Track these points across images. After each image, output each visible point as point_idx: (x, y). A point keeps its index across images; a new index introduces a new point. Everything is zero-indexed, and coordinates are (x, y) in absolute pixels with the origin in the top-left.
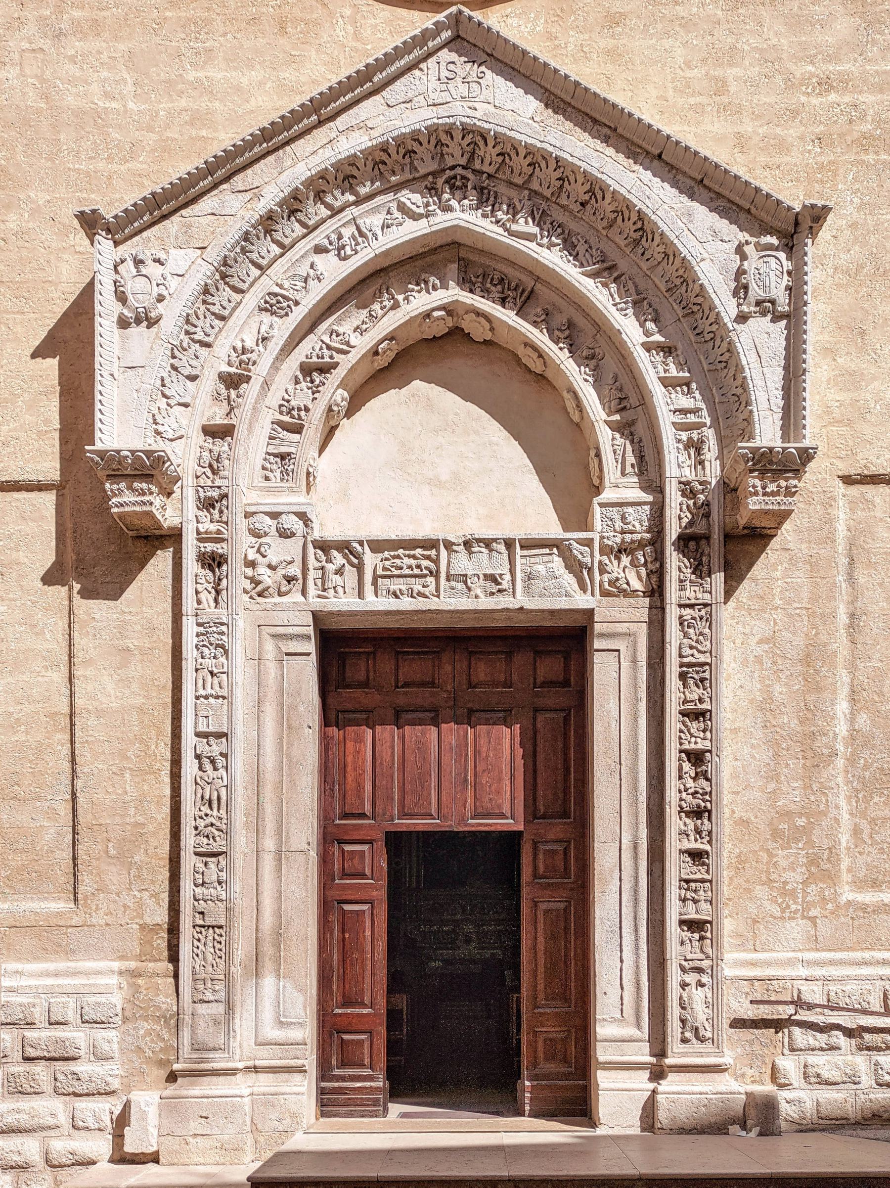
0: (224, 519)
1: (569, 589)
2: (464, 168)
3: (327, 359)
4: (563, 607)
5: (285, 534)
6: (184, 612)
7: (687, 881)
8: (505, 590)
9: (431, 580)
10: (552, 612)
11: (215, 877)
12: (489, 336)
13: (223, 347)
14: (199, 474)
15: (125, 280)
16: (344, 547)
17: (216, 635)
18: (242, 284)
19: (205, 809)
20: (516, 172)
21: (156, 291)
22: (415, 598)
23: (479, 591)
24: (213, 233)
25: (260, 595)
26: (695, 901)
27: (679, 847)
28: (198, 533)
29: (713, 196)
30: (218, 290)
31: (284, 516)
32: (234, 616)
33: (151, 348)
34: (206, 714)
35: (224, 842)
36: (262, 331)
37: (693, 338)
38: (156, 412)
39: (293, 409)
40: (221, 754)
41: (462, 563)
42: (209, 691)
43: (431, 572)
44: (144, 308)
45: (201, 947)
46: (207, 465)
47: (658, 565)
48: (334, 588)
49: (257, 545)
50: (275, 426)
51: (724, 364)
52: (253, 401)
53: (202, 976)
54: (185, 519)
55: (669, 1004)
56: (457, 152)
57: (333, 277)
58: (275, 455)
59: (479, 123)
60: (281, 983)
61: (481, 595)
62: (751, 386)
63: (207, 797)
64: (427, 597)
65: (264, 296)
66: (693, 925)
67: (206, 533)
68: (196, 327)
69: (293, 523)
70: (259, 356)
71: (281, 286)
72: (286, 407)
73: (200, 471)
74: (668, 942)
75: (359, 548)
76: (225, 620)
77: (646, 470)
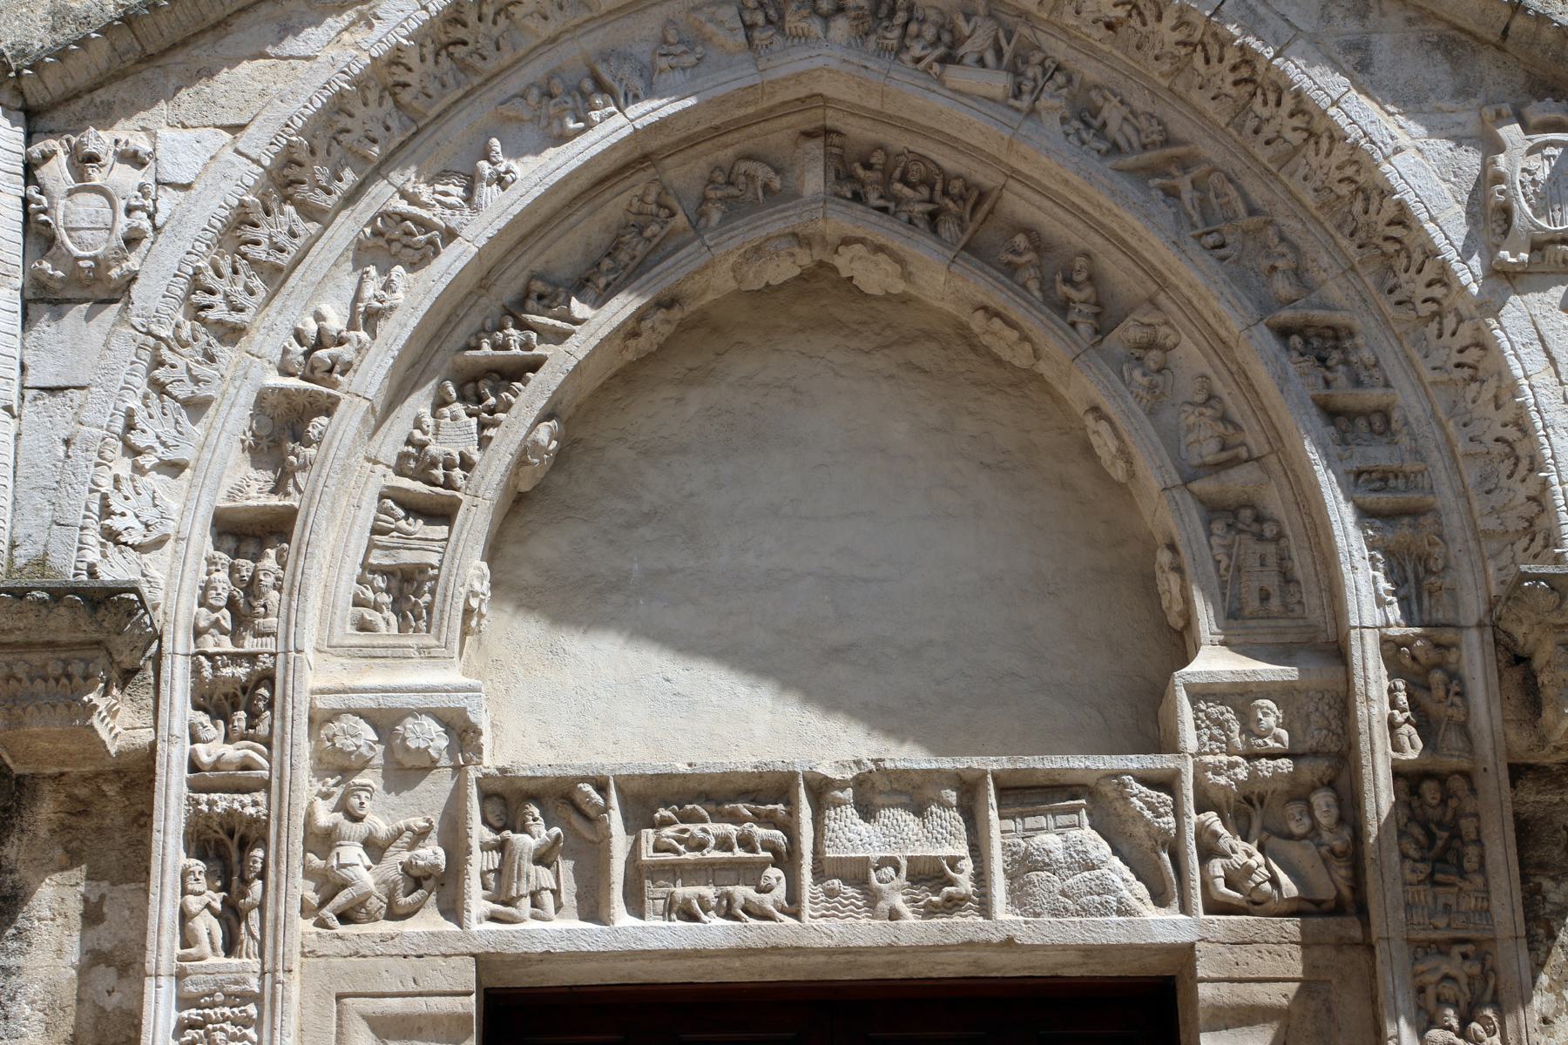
0: (263, 729)
1: (1126, 893)
3: (516, 350)
4: (1113, 941)
5: (405, 771)
6: (150, 967)
8: (966, 898)
9: (773, 873)
10: (1088, 951)
12: (899, 287)
14: (203, 624)
15: (50, 198)
16: (558, 796)
17: (228, 1026)
18: (325, 196)
22: (737, 918)
23: (899, 901)
25: (344, 918)
28: (194, 766)
30: (268, 213)
31: (409, 722)
32: (280, 975)
33: (106, 345)
37: (1389, 309)
38: (106, 485)
39: (434, 464)
41: (853, 835)
43: (775, 851)
44: (94, 258)
46: (223, 603)
47: (1346, 834)
48: (534, 895)
49: (339, 791)
50: (390, 503)
51: (1467, 372)
52: (341, 454)
54: (163, 733)
57: (535, 178)
61: (905, 909)
62: (1539, 425)
64: (767, 916)
65: (374, 219)
67: (215, 767)
69: (428, 735)
70: (358, 351)
71: (413, 200)
72: (416, 461)
76: (254, 985)
77: (1300, 602)
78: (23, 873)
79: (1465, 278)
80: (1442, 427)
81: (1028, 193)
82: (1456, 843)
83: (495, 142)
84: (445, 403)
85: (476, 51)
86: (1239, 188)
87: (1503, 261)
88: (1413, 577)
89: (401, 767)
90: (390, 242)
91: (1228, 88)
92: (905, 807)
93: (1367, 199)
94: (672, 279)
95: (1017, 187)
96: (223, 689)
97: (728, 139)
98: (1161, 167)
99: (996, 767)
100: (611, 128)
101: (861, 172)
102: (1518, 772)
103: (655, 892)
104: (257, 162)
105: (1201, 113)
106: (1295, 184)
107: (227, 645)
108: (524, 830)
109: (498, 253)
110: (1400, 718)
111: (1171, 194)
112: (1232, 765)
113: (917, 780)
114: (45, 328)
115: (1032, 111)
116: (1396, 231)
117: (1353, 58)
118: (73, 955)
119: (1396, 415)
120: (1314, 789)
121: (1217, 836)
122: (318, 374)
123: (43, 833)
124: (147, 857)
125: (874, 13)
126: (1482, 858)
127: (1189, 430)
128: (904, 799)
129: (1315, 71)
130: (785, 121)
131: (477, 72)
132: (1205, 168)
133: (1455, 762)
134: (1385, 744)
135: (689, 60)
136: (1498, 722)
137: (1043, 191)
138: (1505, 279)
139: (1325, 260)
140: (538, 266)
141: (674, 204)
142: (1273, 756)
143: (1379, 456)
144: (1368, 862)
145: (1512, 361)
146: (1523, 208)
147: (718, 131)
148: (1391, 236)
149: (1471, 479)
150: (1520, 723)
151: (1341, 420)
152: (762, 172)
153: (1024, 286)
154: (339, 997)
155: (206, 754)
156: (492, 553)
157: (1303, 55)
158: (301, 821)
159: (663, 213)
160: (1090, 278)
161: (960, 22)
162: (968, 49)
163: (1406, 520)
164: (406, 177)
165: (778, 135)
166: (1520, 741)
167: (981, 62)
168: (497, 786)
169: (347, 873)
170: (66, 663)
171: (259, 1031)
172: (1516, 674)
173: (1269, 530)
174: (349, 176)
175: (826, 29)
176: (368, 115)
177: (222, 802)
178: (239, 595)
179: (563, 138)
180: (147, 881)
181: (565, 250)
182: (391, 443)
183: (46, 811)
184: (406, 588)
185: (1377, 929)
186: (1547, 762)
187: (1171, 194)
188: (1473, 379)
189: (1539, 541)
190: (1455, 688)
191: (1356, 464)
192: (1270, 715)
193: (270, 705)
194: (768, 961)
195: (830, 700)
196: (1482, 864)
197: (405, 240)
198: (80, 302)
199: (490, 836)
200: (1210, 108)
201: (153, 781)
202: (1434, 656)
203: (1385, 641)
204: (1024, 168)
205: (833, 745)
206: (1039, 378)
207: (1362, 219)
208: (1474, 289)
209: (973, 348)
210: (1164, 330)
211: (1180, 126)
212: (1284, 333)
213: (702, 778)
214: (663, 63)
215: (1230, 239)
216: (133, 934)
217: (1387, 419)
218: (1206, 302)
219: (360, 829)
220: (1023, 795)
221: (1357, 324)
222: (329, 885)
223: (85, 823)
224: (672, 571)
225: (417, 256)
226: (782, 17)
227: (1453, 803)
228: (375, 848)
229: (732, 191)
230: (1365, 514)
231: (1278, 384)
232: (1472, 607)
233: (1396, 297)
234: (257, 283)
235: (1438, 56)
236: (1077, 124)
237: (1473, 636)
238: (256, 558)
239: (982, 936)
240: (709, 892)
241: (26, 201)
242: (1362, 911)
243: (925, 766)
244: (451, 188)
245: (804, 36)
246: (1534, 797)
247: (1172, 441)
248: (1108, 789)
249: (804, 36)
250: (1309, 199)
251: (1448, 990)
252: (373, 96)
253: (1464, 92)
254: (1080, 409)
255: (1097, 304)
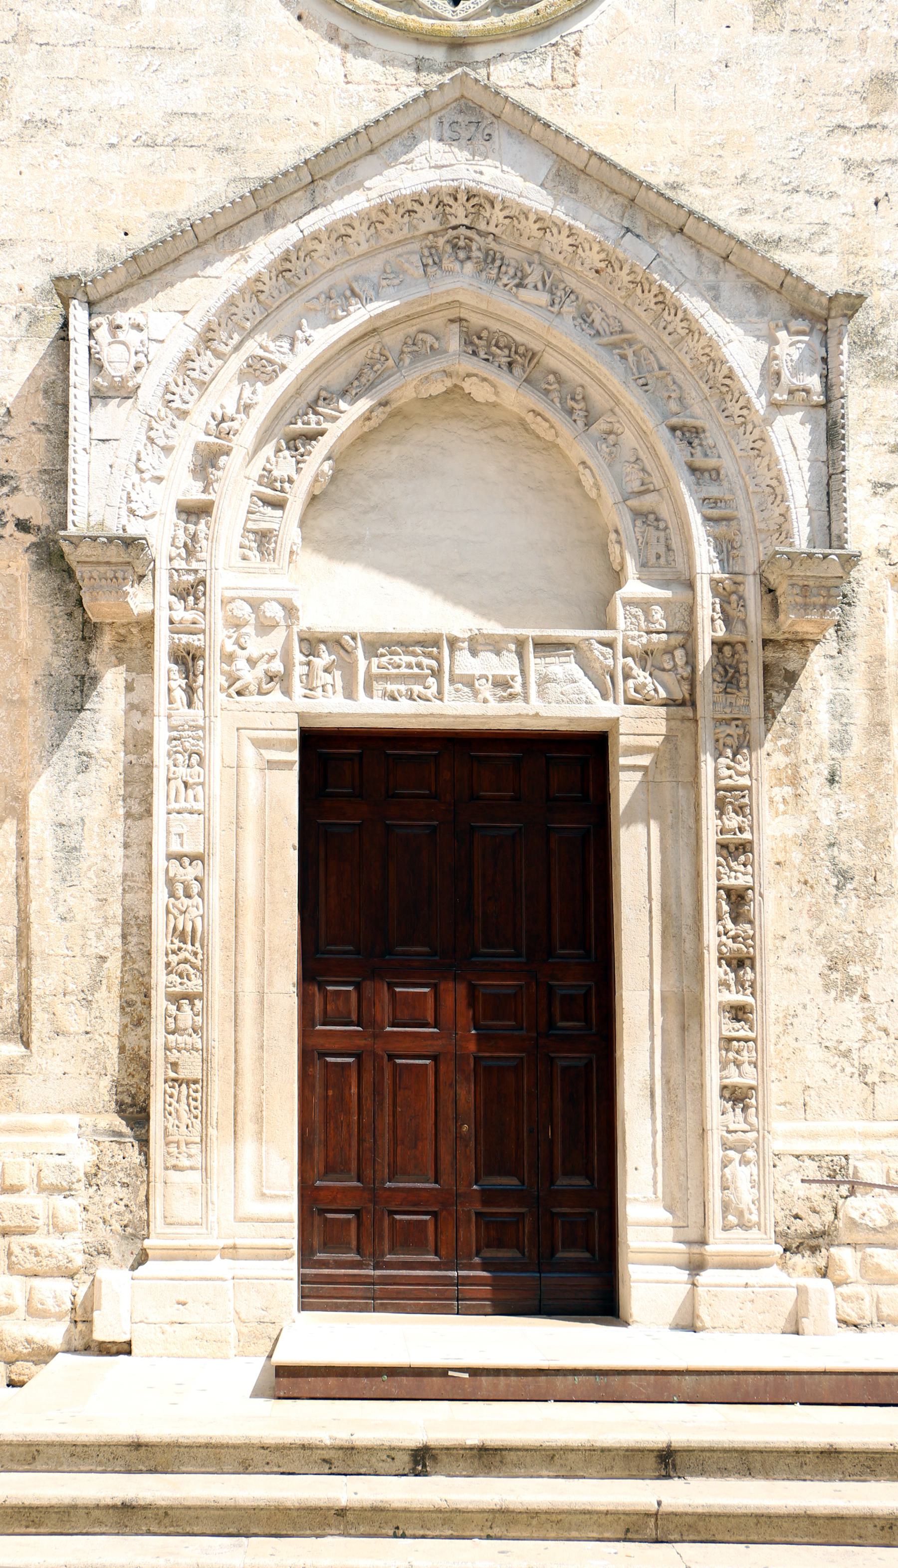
0: (201, 605)
2: (468, 228)
5: (265, 627)
6: (156, 712)
7: (730, 1040)
9: (431, 681)
10: (571, 720)
11: (190, 1023)
12: (493, 399)
13: (201, 414)
14: (173, 555)
16: (335, 642)
19: (177, 943)
20: (525, 236)
21: (134, 360)
24: (196, 295)
25: (239, 693)
26: (738, 1065)
27: (719, 999)
28: (171, 622)
29: (740, 273)
31: (266, 604)
32: (212, 718)
34: (180, 831)
35: (200, 981)
36: (245, 396)
37: (722, 420)
38: (129, 488)
39: (276, 481)
40: (196, 879)
41: (466, 664)
42: (182, 805)
43: (432, 670)
44: (121, 377)
45: (174, 1103)
47: (689, 669)
49: (235, 635)
50: (255, 499)
51: (756, 452)
53: (175, 1138)
54: (157, 605)
55: (711, 1182)
56: (461, 213)
58: (255, 532)
59: (485, 188)
60: (264, 1148)
61: (490, 698)
63: (181, 928)
66: (736, 1096)
68: (174, 394)
69: (274, 611)
71: (265, 349)
72: (267, 478)
73: (174, 552)
74: (708, 1109)
75: (352, 643)
76: (201, 722)
78: (99, 667)
79: (758, 406)
80: (743, 478)
81: (555, 354)
82: (737, 675)
83: (304, 321)
84: (280, 451)
85: (296, 275)
86: (655, 356)
87: (775, 399)
88: (726, 550)
89: (262, 625)
90: (255, 370)
91: (652, 306)
92: (491, 651)
93: (715, 365)
94: (387, 392)
95: (550, 351)
96: (182, 586)
97: (414, 322)
98: (619, 343)
99: (534, 634)
100: (359, 316)
101: (476, 341)
102: (766, 642)
103: (378, 687)
104: (194, 329)
105: (639, 318)
106: (681, 355)
107: (183, 565)
108: (319, 656)
109: (306, 376)
110: (716, 616)
111: (623, 357)
112: (640, 636)
113: (498, 639)
114: (99, 408)
115: (559, 313)
116: (727, 381)
117: (712, 293)
118: (122, 705)
119: (722, 472)
120: (676, 648)
121: (631, 669)
122: (223, 435)
123: (106, 649)
124: (152, 663)
125: (485, 261)
126: (748, 682)
127: (627, 475)
128: (491, 648)
129: (694, 299)
130: (441, 314)
131: (296, 286)
132: (640, 345)
133: (739, 638)
134: (709, 630)
135: (396, 281)
136: (759, 620)
137: (562, 353)
138: (776, 406)
139: (694, 394)
140: (323, 384)
141: (388, 354)
142: (658, 633)
143: (714, 491)
144: (698, 683)
145: (777, 448)
146: (786, 374)
147: (409, 318)
148: (723, 384)
149: (755, 504)
150: (769, 620)
151: (698, 473)
152: (430, 339)
153: (552, 401)
154: (238, 729)
155: (177, 616)
156: (302, 524)
157: (688, 291)
158: (218, 649)
159: (383, 358)
160: (583, 398)
161: (526, 266)
162: (529, 281)
163: (724, 523)
164: (262, 338)
165: (437, 321)
166: (769, 630)
167: (536, 287)
168: (306, 636)
169: (239, 673)
170: (115, 572)
171: (204, 742)
172: (769, 597)
173: (662, 525)
174: (237, 337)
175: (462, 268)
176: (246, 306)
177: (185, 639)
178: (189, 542)
179: (336, 320)
180: (152, 673)
181: (336, 377)
182: (256, 470)
183: (107, 639)
184: (263, 539)
185: (700, 713)
186: (779, 638)
187: (623, 357)
188: (758, 456)
189: (784, 535)
190: (741, 603)
191: (703, 495)
192: (658, 613)
193: (204, 594)
194: (427, 720)
195: (456, 599)
196: (747, 685)
197: (262, 369)
198: (114, 398)
199: (304, 659)
200: (643, 315)
201: (153, 627)
202: (733, 588)
203: (712, 580)
204: (554, 341)
205: (458, 621)
206: (557, 446)
207: (712, 374)
208: (762, 412)
209: (527, 430)
210: (617, 425)
211: (629, 324)
212: (673, 429)
213: (399, 635)
214: (384, 283)
215: (650, 382)
216: (147, 697)
217: (718, 474)
218: (639, 417)
219: (245, 653)
220: (544, 646)
221: (707, 426)
222: (233, 679)
223: (124, 645)
224: (384, 535)
225: (268, 377)
226: (441, 261)
227: (737, 656)
228: (252, 662)
229: (415, 348)
230: (707, 519)
231: (670, 455)
232: (752, 566)
233: (726, 413)
234: (194, 390)
235: (751, 294)
236: (580, 321)
237: (751, 578)
238: (196, 524)
239: (525, 712)
240: (403, 688)
241: (90, 348)
242: (693, 704)
243: (501, 632)
244: (283, 344)
245: (450, 271)
246: (772, 654)
247: (619, 480)
248: (584, 646)
249: (450, 271)
250: (688, 363)
251: (729, 741)
252: (247, 297)
253: (762, 314)
254: (576, 462)
255: (586, 411)
